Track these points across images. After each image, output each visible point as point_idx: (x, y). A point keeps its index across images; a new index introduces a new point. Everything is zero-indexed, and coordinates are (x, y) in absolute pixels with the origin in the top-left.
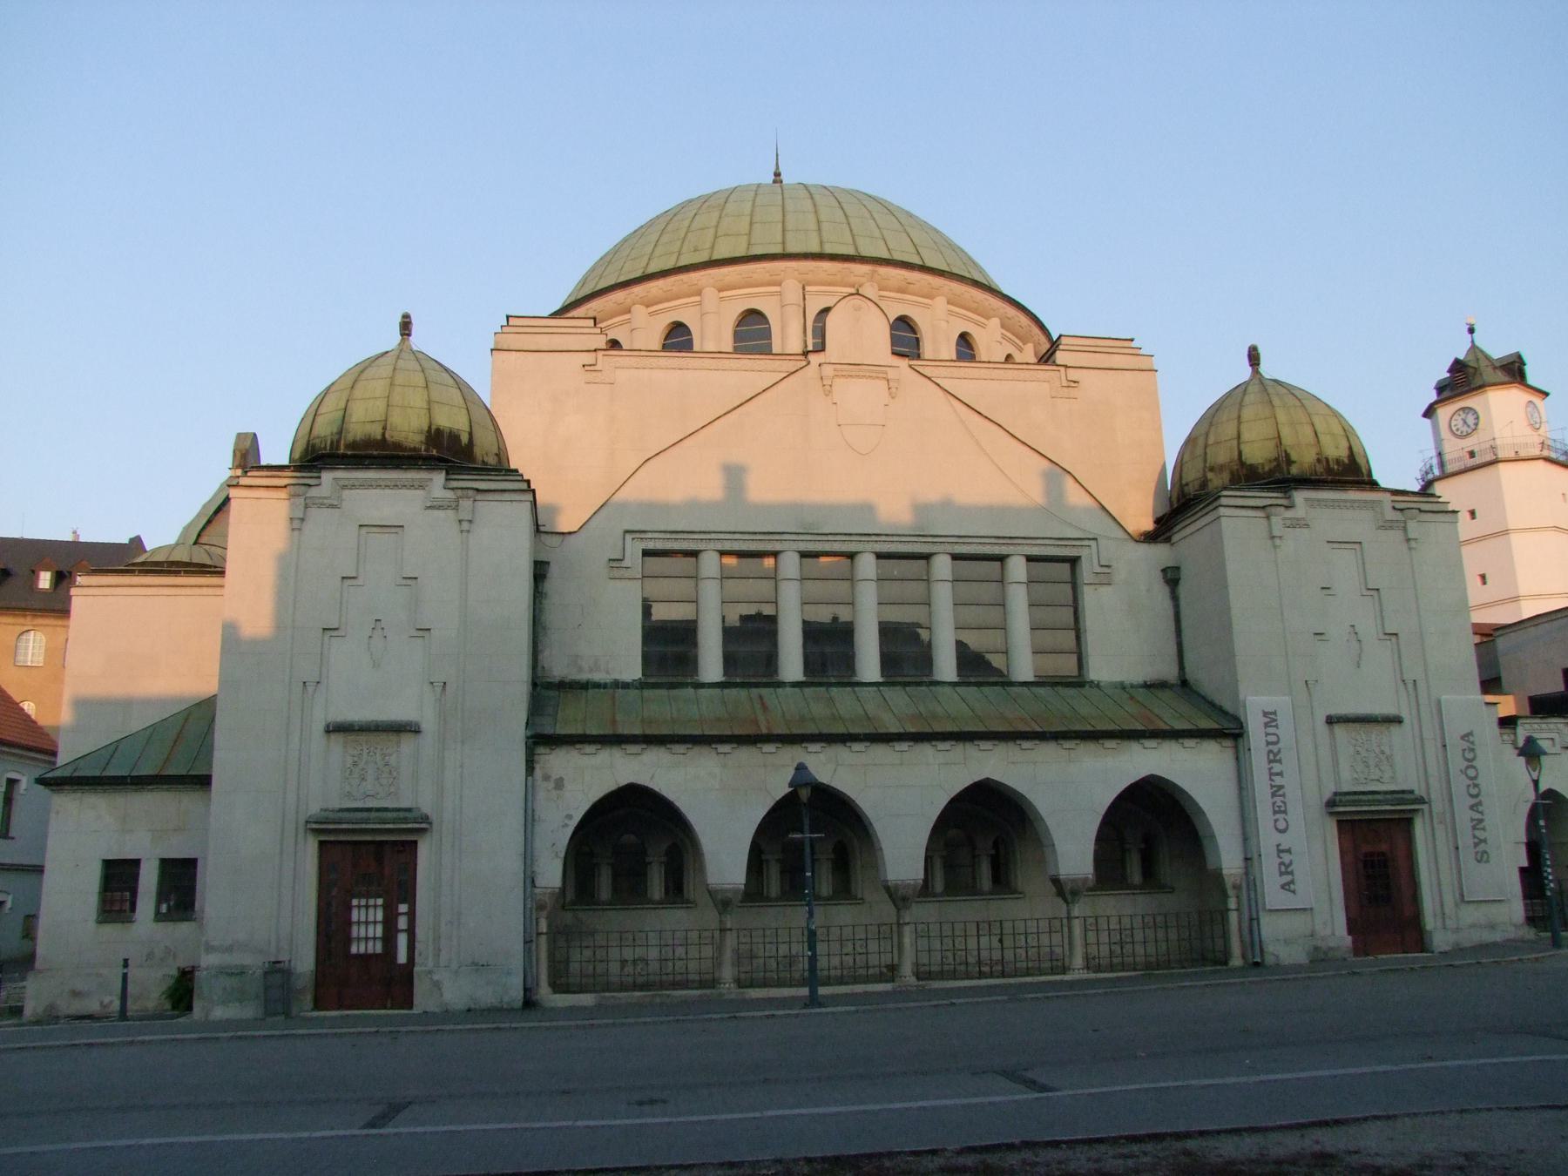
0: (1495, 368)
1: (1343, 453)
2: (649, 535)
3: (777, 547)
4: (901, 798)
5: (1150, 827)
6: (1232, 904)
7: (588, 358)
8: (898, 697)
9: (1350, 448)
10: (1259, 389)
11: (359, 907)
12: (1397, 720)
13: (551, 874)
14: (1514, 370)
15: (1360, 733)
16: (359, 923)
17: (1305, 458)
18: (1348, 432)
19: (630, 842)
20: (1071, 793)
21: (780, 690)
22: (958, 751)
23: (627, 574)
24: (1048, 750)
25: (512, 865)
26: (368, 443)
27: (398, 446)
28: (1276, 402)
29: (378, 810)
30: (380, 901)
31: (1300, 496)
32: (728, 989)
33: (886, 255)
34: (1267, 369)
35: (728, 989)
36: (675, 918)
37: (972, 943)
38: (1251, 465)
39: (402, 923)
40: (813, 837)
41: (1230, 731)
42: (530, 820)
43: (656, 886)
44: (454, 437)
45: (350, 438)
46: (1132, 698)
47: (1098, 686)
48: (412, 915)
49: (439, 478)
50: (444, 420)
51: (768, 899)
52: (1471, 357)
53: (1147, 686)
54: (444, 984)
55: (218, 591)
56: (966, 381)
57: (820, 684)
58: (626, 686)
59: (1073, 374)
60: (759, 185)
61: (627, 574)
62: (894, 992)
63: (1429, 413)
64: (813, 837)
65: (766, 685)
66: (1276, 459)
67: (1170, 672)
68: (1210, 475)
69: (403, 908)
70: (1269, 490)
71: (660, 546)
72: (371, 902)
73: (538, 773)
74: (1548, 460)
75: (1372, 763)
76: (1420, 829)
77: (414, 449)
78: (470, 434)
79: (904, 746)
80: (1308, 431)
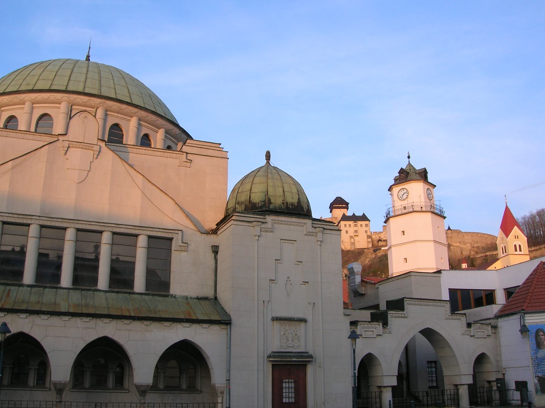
0: (416, 173)
2: (34, 217)
3: (29, 222)
5: (184, 361)
8: (76, 297)
9: (299, 199)
10: (268, 170)
12: (304, 321)
14: (423, 175)
17: (277, 201)
18: (300, 191)
20: (145, 345)
21: (21, 288)
24: (137, 325)
28: (270, 176)
31: (270, 219)
33: (113, 96)
34: (273, 162)
36: (40, 396)
38: (254, 203)
41: (225, 322)
46: (188, 304)
47: (175, 297)
51: (182, 390)
52: (408, 168)
56: (140, 156)
59: (190, 157)
60: (77, 61)
63: (390, 189)
66: (265, 201)
67: (209, 293)
68: (237, 206)
71: (9, 220)
74: (433, 213)
75: (290, 339)
79: (66, 318)
80: (281, 190)
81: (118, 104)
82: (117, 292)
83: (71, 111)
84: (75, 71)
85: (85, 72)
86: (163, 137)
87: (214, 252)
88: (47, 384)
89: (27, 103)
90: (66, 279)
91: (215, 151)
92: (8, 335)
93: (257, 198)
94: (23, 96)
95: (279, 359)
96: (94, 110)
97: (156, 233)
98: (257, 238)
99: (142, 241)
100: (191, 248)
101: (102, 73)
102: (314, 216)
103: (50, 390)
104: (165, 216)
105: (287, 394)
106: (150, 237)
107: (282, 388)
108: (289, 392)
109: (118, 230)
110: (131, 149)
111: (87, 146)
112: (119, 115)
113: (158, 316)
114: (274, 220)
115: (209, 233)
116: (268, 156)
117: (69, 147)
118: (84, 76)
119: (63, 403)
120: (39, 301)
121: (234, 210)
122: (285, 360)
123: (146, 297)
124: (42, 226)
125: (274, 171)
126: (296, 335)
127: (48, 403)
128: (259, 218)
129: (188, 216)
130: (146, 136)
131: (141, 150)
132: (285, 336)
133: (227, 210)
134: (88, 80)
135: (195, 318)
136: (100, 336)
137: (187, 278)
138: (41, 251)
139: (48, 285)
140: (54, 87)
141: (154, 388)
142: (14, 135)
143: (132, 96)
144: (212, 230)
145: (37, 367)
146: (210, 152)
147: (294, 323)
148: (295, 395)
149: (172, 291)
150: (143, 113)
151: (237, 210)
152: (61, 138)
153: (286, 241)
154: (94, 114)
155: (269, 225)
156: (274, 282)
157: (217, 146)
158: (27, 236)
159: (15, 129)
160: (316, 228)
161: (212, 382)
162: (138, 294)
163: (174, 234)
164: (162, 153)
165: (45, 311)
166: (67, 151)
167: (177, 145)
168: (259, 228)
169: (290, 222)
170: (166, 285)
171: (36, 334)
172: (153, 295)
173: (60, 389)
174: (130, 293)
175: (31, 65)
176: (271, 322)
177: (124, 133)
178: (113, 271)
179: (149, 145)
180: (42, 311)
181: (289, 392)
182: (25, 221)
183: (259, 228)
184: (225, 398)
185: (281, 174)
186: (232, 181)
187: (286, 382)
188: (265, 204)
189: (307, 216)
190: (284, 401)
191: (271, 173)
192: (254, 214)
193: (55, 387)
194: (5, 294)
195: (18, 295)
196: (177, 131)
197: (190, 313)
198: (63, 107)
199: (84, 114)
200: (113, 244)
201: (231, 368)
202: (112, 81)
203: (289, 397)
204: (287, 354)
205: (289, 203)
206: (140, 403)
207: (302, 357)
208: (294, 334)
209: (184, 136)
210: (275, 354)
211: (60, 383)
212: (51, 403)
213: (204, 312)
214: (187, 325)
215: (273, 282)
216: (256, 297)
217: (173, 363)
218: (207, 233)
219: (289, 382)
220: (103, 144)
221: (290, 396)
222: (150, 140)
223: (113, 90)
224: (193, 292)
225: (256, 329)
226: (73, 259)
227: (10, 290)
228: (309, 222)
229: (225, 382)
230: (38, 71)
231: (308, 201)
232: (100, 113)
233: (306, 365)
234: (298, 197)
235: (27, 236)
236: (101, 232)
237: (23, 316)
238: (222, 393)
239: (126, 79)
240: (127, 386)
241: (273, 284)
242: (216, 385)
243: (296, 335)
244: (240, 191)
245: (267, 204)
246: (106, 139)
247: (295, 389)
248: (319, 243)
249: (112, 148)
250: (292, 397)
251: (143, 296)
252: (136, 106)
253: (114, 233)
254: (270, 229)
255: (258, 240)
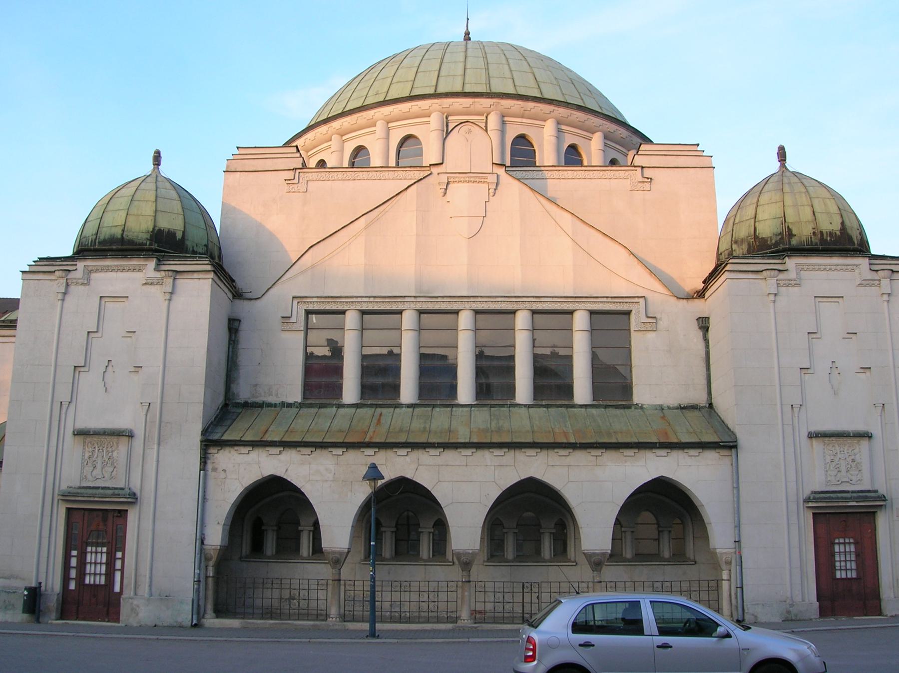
1: (836, 227)
3: (400, 307)
4: (466, 489)
5: (662, 511)
6: (725, 576)
7: (290, 175)
8: (482, 417)
9: (843, 223)
10: (785, 178)
11: (91, 552)
12: (868, 436)
13: (216, 537)
15: (838, 448)
16: (91, 563)
17: (803, 232)
18: (844, 209)
19: (271, 517)
20: (596, 489)
21: (397, 410)
22: (509, 456)
23: (294, 327)
24: (580, 457)
25: (188, 529)
26: (112, 240)
27: (131, 242)
28: (787, 188)
29: (103, 488)
30: (105, 549)
31: (792, 263)
32: (333, 621)
33: (511, 91)
34: (792, 164)
35: (333, 621)
36: (440, 573)
37: (518, 598)
39: (118, 564)
40: (401, 516)
41: (727, 444)
42: (203, 499)
43: (547, 549)
44: (171, 234)
45: (102, 238)
47: (642, 408)
48: (123, 559)
49: (152, 264)
50: (164, 224)
53: (681, 408)
54: (138, 610)
55: (12, 339)
56: (565, 183)
57: (428, 405)
58: (289, 405)
59: (647, 173)
60: (449, 44)
61: (294, 327)
62: (453, 630)
64: (401, 516)
65: (389, 406)
66: (781, 234)
67: (701, 398)
68: (734, 247)
69: (74, 553)
70: (773, 258)
71: (370, 307)
72: (99, 549)
73: (209, 466)
75: (843, 469)
76: (882, 521)
77: (142, 244)
78: (184, 232)
79: (468, 452)
80: (808, 211)
81: (520, 103)
82: (547, 406)
83: (447, 126)
84: (445, 60)
85: (462, 59)
86: (601, 146)
87: (701, 328)
88: (449, 556)
89: (379, 123)
90: (465, 391)
91: (691, 157)
92: (380, 483)
93: (767, 229)
94: (370, 113)
95: (854, 504)
96: (484, 118)
97: (601, 305)
98: (772, 298)
99: (580, 321)
100: (662, 324)
101: (488, 56)
102: (874, 251)
103: (454, 563)
104: (615, 277)
105: (843, 564)
106: (592, 313)
107: (833, 554)
108: (846, 561)
109: (540, 306)
110: (550, 173)
111: (476, 177)
112: (524, 120)
113: (614, 440)
114: (800, 264)
115: (693, 298)
116: (782, 154)
117: (448, 183)
118: (461, 65)
119: (473, 584)
120: (425, 428)
121: (731, 255)
122: (841, 504)
123: (594, 411)
124: (421, 312)
125: (795, 180)
126: (853, 461)
127: (394, 584)
128: (774, 263)
129: (653, 272)
130: (573, 148)
131: (566, 173)
132: (834, 464)
133: (719, 255)
134: (468, 71)
135: (675, 441)
136: (523, 478)
137: (659, 376)
138: (423, 351)
139: (438, 402)
140: (416, 92)
141: (615, 556)
142: (365, 175)
143: (542, 85)
144: (698, 292)
145: (394, 529)
146: (681, 161)
147: (849, 441)
148: (857, 565)
149: (637, 399)
150: (562, 112)
151: (735, 254)
152: (435, 170)
153: (825, 300)
154: (483, 125)
155: (792, 275)
156: (809, 371)
157: (693, 149)
158: (456, 330)
159: (366, 165)
160: (877, 271)
161: (711, 546)
162: (581, 406)
163: (631, 305)
164: (602, 173)
165: (434, 443)
166: (446, 189)
167: (626, 155)
168: (774, 281)
169: (830, 265)
170: (627, 389)
171: (424, 479)
172: (606, 407)
173: (338, 561)
174: (567, 406)
175: (379, 63)
176: (808, 440)
177: (536, 148)
178: (480, 372)
179: (580, 163)
180: (494, 443)
181: (846, 561)
182: (394, 307)
183: (774, 281)
184: (733, 571)
185: (806, 184)
186: (725, 204)
187: (839, 544)
188: (782, 238)
189: (860, 251)
190: (838, 576)
191: (789, 183)
192: (763, 257)
193: (459, 559)
194: (375, 421)
195: (393, 421)
196: (623, 132)
197: (666, 433)
198: (435, 121)
199: (466, 127)
200: (420, 329)
201: (742, 521)
202: (506, 67)
203: (846, 570)
204: (839, 495)
205: (824, 232)
206: (593, 582)
207: (865, 499)
208: (849, 459)
209: (637, 140)
210: (816, 496)
211: (466, 554)
212: (454, 584)
213: (691, 430)
214: (663, 452)
215: (805, 371)
216: (778, 396)
217: (647, 516)
218: (689, 297)
219: (844, 543)
220: (501, 171)
221: (848, 567)
222: (579, 155)
223: (510, 81)
224: (671, 397)
225: (782, 453)
226: (418, 356)
227: (381, 414)
228: (864, 262)
229: (732, 545)
230: (389, 71)
231: (860, 225)
232: (493, 121)
233: (874, 513)
234: (840, 221)
235: (456, 329)
236: (513, 312)
237: (403, 452)
238: (729, 563)
239: (529, 60)
240: (573, 555)
241: (807, 376)
242: (718, 551)
243: (853, 461)
244: (737, 221)
245: (786, 239)
246: (508, 163)
247: (857, 555)
248: (885, 297)
249: (519, 175)
250: (851, 570)
251: (589, 410)
252: (550, 102)
253: (534, 312)
254: (795, 280)
255: (774, 302)
